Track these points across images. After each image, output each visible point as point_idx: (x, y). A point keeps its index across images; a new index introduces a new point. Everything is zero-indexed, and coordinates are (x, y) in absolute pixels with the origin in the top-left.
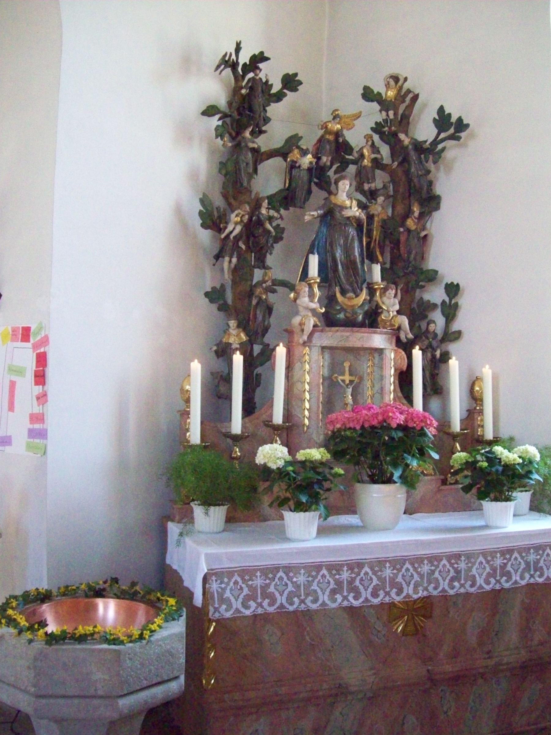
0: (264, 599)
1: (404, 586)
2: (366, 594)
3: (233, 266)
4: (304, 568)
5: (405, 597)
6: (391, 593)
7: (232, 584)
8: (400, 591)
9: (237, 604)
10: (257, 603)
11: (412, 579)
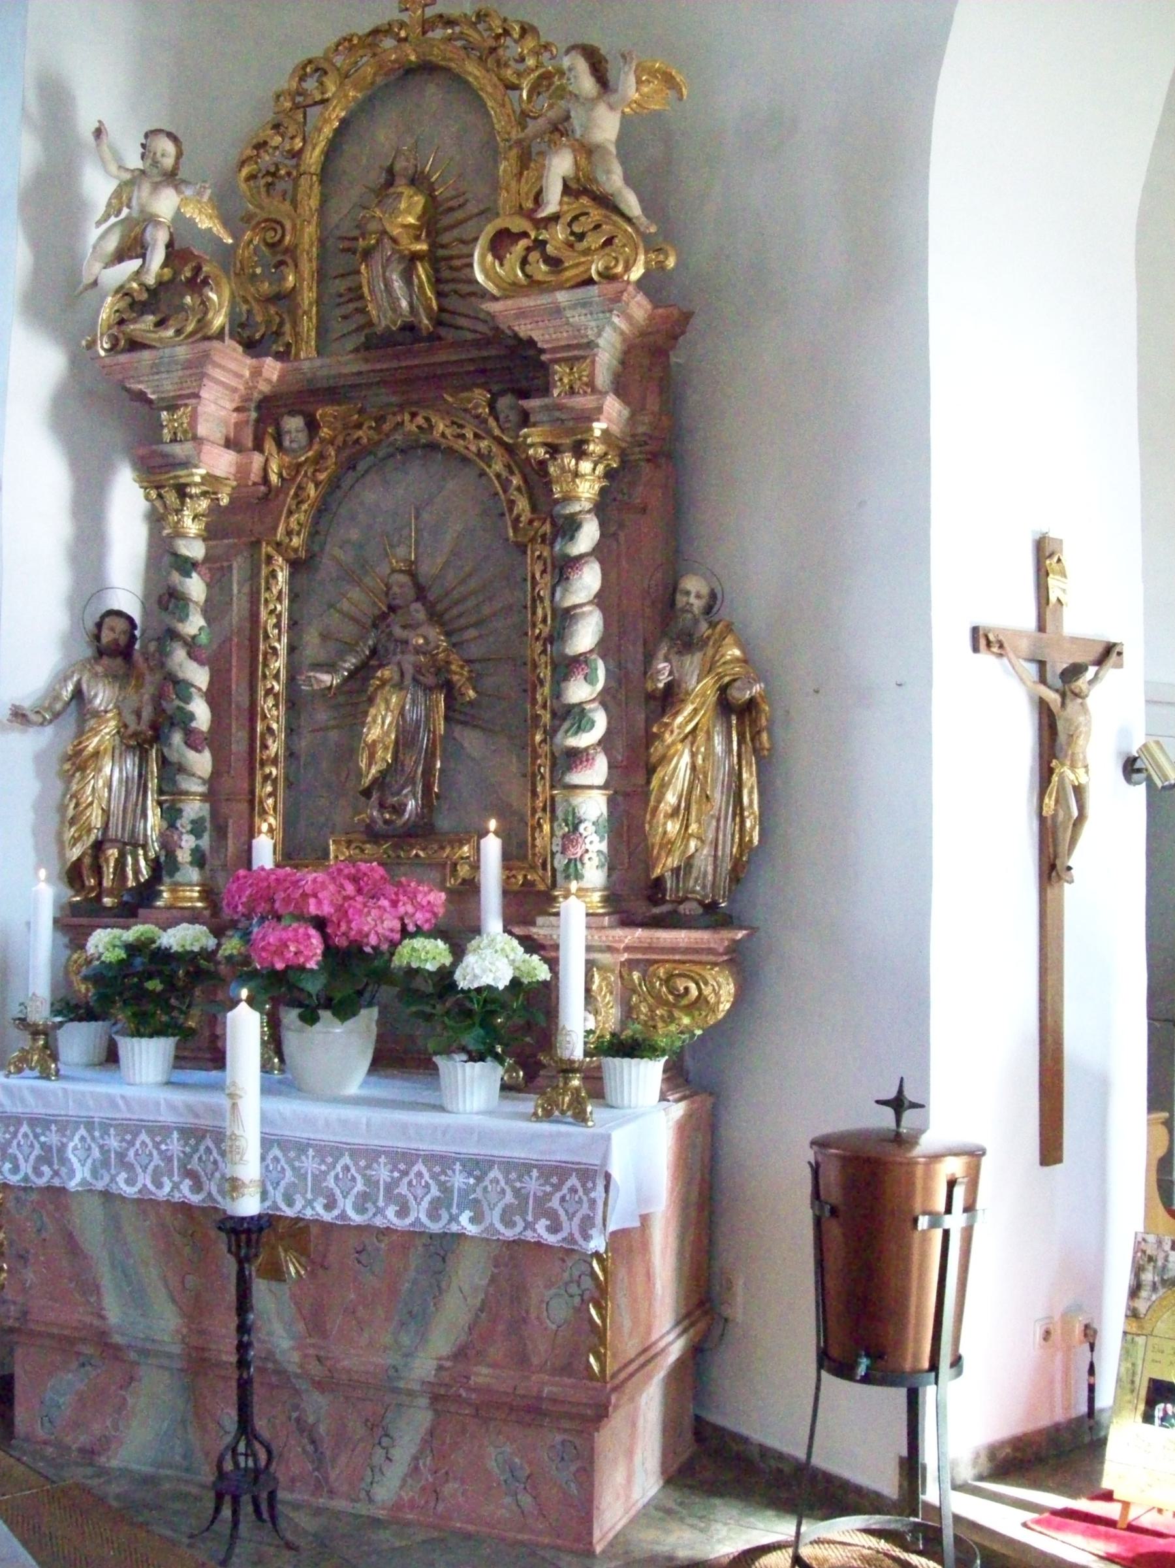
0: (462, 1211)
1: (412, 1203)
2: (145, 1179)
3: (227, 618)
4: (116, 1127)
5: (412, 1225)
6: (461, 1219)
7: (339, 1168)
8: (403, 1212)
9: (26, 1168)
10: (52, 1169)
11: (427, 1193)
